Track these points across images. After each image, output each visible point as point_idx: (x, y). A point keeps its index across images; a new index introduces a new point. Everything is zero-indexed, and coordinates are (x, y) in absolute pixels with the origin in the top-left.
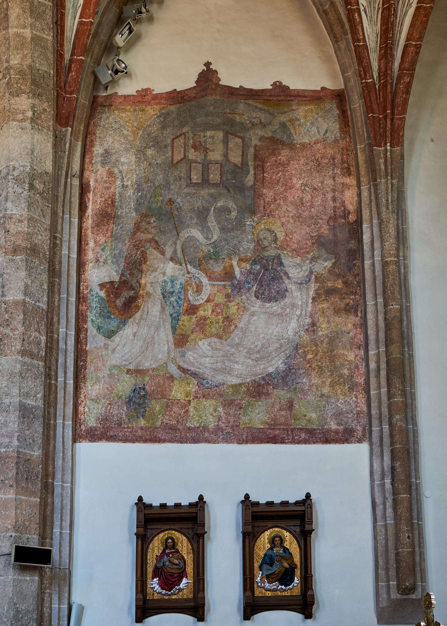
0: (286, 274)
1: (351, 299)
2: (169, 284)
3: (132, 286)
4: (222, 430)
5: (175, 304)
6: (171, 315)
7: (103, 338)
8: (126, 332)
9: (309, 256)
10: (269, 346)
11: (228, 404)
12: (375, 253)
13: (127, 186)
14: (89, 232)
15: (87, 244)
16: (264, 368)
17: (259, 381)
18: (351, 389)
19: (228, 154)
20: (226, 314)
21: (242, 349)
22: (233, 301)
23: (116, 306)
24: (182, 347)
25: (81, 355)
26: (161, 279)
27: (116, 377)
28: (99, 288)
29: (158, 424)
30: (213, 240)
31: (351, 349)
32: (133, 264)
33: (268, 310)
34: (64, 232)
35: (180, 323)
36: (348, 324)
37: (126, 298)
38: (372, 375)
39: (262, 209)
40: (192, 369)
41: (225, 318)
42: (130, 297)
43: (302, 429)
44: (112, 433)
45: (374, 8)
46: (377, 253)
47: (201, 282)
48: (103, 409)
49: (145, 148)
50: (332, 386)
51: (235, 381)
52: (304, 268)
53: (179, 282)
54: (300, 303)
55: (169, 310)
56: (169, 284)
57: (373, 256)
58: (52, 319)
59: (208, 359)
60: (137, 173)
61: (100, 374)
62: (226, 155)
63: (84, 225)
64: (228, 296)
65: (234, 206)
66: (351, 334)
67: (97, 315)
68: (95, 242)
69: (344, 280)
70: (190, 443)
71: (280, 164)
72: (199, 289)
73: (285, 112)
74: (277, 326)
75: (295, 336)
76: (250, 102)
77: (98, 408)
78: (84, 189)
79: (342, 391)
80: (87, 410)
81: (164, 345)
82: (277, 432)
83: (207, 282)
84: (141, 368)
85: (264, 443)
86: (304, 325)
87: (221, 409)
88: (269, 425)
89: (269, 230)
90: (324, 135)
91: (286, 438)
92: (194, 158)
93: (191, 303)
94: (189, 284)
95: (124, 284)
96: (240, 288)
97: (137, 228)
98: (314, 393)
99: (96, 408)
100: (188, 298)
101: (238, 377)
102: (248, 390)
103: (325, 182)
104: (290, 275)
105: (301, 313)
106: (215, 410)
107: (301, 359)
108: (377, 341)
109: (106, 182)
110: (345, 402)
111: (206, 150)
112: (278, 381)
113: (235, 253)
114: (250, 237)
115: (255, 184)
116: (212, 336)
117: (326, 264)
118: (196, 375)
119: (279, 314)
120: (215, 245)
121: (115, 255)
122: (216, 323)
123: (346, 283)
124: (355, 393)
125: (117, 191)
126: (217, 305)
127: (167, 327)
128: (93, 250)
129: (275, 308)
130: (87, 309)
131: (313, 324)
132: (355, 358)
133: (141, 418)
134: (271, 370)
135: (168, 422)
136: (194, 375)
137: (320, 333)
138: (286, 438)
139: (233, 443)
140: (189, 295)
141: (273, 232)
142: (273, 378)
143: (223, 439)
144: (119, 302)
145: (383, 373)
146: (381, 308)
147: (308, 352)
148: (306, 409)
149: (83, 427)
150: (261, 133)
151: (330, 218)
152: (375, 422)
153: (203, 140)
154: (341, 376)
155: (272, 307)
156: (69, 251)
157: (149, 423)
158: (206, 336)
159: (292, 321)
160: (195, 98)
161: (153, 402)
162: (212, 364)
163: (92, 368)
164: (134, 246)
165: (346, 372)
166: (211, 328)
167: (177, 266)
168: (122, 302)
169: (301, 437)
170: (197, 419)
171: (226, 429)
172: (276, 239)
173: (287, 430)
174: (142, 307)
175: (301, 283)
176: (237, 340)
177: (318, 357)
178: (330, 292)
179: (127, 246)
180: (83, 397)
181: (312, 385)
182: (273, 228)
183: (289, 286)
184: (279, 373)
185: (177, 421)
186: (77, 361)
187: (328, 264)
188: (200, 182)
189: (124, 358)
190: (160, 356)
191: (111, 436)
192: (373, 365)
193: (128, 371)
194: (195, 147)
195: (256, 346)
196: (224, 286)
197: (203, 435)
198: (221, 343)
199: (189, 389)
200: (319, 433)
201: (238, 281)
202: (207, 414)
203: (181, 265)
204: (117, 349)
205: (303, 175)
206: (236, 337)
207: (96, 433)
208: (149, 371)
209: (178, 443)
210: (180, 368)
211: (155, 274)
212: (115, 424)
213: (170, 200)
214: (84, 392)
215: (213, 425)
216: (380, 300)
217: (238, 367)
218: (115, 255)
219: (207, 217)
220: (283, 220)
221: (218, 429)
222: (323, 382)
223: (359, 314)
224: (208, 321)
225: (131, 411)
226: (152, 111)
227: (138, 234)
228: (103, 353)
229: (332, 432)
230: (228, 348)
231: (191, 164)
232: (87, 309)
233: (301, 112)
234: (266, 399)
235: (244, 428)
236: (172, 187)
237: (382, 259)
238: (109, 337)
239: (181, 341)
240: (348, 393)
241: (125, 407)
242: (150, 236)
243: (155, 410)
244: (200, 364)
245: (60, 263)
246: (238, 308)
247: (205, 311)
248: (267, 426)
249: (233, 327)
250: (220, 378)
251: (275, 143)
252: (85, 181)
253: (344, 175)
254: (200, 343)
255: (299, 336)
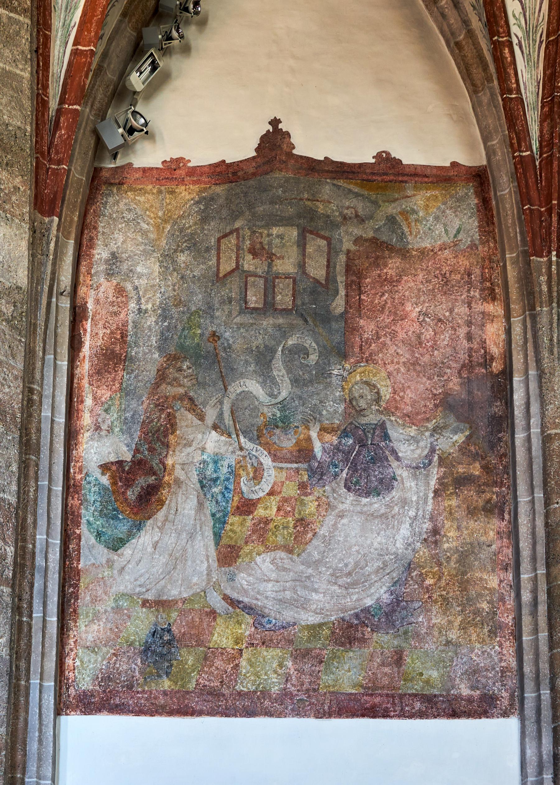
0: (394, 452)
1: (493, 493)
2: (211, 466)
3: (152, 468)
4: (291, 696)
5: (220, 498)
6: (213, 515)
7: (106, 550)
8: (141, 540)
9: (430, 425)
10: (367, 565)
11: (301, 655)
12: (532, 421)
13: (146, 311)
14: (85, 383)
15: (82, 402)
16: (358, 600)
17: (350, 619)
18: (493, 633)
19: (305, 263)
20: (300, 514)
21: (324, 569)
22: (310, 494)
23: (126, 499)
24: (230, 565)
25: (69, 577)
26: (198, 458)
27: (126, 611)
28: (100, 471)
29: (192, 686)
30: (280, 399)
31: (493, 571)
32: (153, 434)
33: (365, 509)
34: (45, 382)
35: (228, 527)
36: (489, 530)
37: (142, 487)
38: (525, 611)
39: (357, 350)
40: (246, 600)
41: (298, 520)
42: (149, 486)
43: (415, 695)
44: (117, 701)
45: (534, 40)
46: (535, 421)
47: (262, 464)
48: (104, 663)
49: (176, 251)
50: (463, 628)
51: (312, 619)
52: (422, 444)
53: (225, 463)
54: (414, 498)
55: (210, 507)
56: (211, 466)
57: (528, 427)
58: (25, 519)
59: (270, 585)
60: (163, 290)
61: (100, 608)
62: (302, 266)
63: (77, 371)
64: (302, 486)
65: (314, 344)
66: (494, 547)
67: (96, 513)
68: (95, 398)
69: (483, 462)
70: (241, 716)
71: (385, 280)
72: (257, 475)
73: (395, 200)
74: (378, 534)
75: (406, 549)
76: (341, 183)
77: (96, 660)
78: (78, 315)
79: (478, 636)
80: (78, 663)
81: (202, 562)
82: (377, 700)
83: (270, 463)
84: (165, 598)
85: (358, 716)
86: (420, 533)
87: (289, 664)
88: (365, 688)
89: (367, 383)
90: (455, 236)
91: (392, 709)
92: (252, 268)
93: (245, 496)
94: (241, 466)
95: (139, 465)
96: (322, 474)
97: (162, 376)
98: (435, 639)
99: (92, 660)
100: (241, 489)
101: (317, 613)
102: (333, 633)
103: (456, 310)
104: (400, 455)
105: (417, 514)
106: (281, 665)
107: (416, 586)
108: (534, 559)
109: (112, 304)
110: (483, 652)
111: (271, 257)
112: (379, 619)
113: (315, 419)
114: (338, 394)
115: (346, 312)
116: (277, 548)
117: (455, 438)
118: (252, 609)
119: (383, 514)
120: (283, 406)
121: (126, 419)
122: (284, 528)
123: (486, 468)
124: (498, 639)
125: (130, 318)
126: (285, 500)
127: (206, 534)
128: (91, 411)
129: (376, 506)
130: (81, 504)
131: (435, 531)
132: (499, 585)
133: (165, 676)
134: (369, 602)
135: (207, 683)
136: (249, 609)
137: (446, 546)
138: (392, 709)
139: (309, 716)
140: (242, 484)
141: (375, 386)
142: (373, 615)
143: (293, 710)
144: (131, 495)
145: (542, 609)
146: (539, 507)
147: (427, 575)
148: (422, 664)
149: (72, 691)
150: (357, 231)
151: (463, 366)
152: (529, 685)
153: (265, 240)
154: (477, 612)
155: (371, 504)
156: (52, 413)
157: (176, 684)
158: (268, 549)
159: (403, 526)
160: (254, 174)
161: (184, 651)
162: (276, 592)
163: (88, 598)
164: (157, 406)
165: (485, 606)
166: (276, 537)
167: (223, 438)
168: (136, 493)
169: (414, 708)
170: (253, 678)
171: (297, 695)
172: (378, 399)
173: (393, 696)
174: (167, 502)
175: (417, 468)
176: (316, 556)
177: (443, 583)
178: (461, 482)
179: (145, 406)
180: (73, 644)
181: (433, 627)
182: (374, 380)
183: (399, 472)
184: (381, 608)
185: (221, 682)
186: (64, 586)
187: (460, 438)
188: (261, 306)
189: (138, 583)
190: (195, 580)
191: (117, 706)
192: (526, 596)
193: (145, 603)
194: (254, 252)
195: (346, 565)
196: (297, 470)
197: (261, 703)
198: (291, 559)
199: (240, 631)
200: (443, 701)
201: (319, 462)
202: (268, 670)
203: (229, 436)
204: (127, 568)
205: (422, 299)
206: (314, 550)
207: (93, 700)
208: (177, 602)
209: (222, 716)
210: (226, 598)
211: (189, 450)
212: (123, 687)
213: (214, 334)
214: (75, 636)
215: (276, 688)
216: (539, 495)
217: (317, 598)
218: (126, 419)
219: (271, 361)
220: (390, 368)
221: (285, 694)
222: (450, 622)
223: (507, 516)
224: (271, 526)
225: (149, 666)
226: (187, 194)
227: (163, 386)
228: (106, 574)
229: (462, 699)
230: (302, 567)
231: (246, 278)
232: (81, 504)
233: (419, 199)
234: (360, 648)
235: (325, 693)
236: (218, 314)
237: (543, 432)
238: (115, 549)
239: (229, 555)
240: (487, 640)
241: (139, 660)
242: (181, 390)
243: (186, 664)
244: (258, 593)
245: (39, 430)
246: (319, 505)
247: (266, 509)
248: (362, 691)
249: (310, 535)
250: (288, 615)
251: (379, 248)
252: (79, 302)
253: (485, 300)
254: (259, 559)
255: (414, 550)
